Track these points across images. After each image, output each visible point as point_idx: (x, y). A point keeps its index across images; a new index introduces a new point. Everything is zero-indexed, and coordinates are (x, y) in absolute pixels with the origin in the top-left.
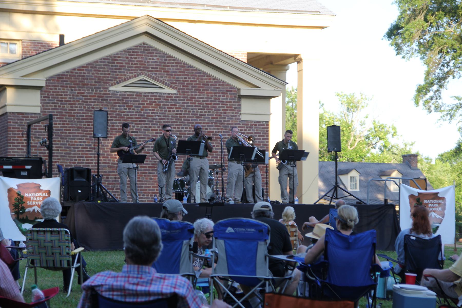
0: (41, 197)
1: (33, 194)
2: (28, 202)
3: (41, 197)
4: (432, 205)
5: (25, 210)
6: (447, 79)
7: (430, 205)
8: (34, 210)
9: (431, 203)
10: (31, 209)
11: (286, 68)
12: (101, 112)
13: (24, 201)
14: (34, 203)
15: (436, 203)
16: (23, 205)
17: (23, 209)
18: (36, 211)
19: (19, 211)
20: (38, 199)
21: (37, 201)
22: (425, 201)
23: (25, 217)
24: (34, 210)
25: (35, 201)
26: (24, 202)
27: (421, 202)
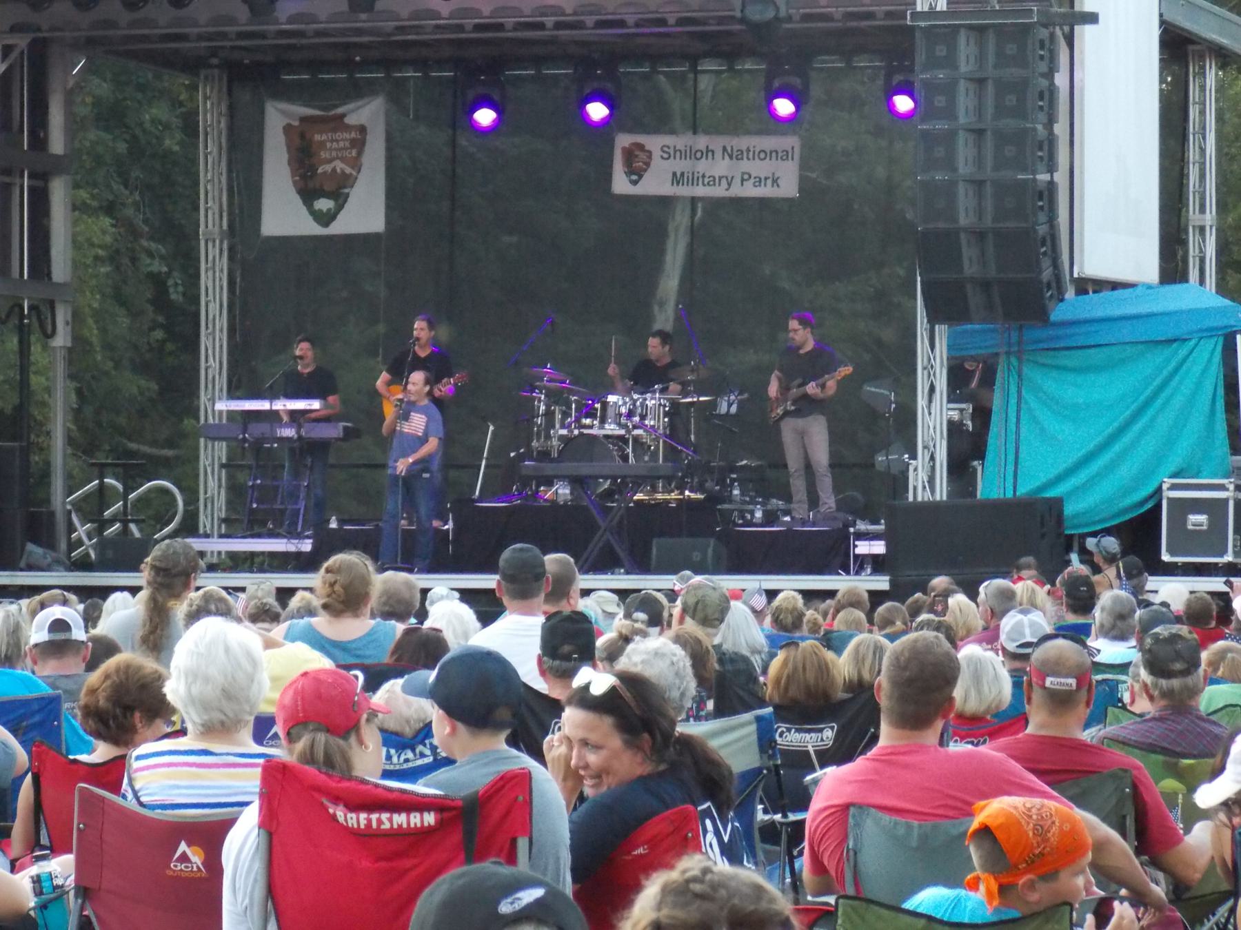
7: (328, 145)
8: (334, 170)
9: (332, 141)
14: (334, 154)
20: (341, 144)
22: (317, 137)
24: (334, 170)
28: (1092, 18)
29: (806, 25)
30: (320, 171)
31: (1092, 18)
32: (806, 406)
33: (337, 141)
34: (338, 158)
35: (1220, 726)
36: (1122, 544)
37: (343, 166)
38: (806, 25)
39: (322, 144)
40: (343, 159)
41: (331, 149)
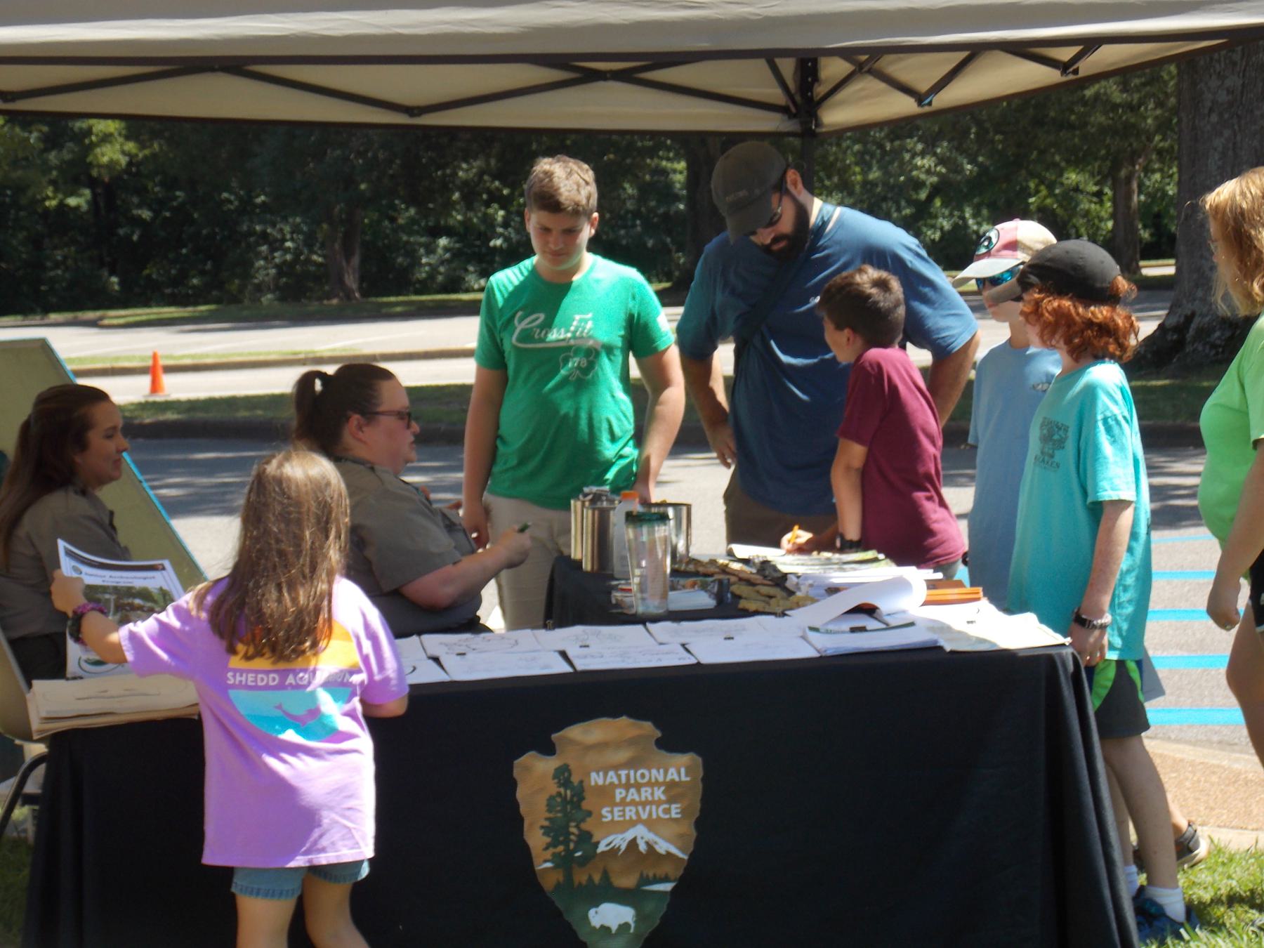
0: (657, 784)
1: (623, 773)
2: (604, 811)
3: (657, 784)
4: (633, 795)
5: (597, 844)
6: (1066, 343)
7: (619, 794)
8: (633, 843)
9: (627, 786)
10: (620, 841)
11: (654, 279)
12: (1082, 516)
13: (586, 805)
14: (630, 813)
15: (650, 784)
16: (584, 826)
17: (586, 838)
18: (642, 847)
19: (570, 853)
20: (646, 793)
21: (644, 804)
22: (596, 779)
23: (597, 878)
24: (633, 843)
25: (633, 803)
26: (589, 814)
27: (575, 780)
28: (155, 357)
29: (160, 508)
30: (602, 848)
31: (155, 357)
32: (1169, 515)
33: (638, 787)
34: (639, 821)
35: (367, 626)
36: (68, 206)
37: (650, 836)
38: (160, 508)
39: (606, 793)
40: (650, 824)
41: (623, 803)
